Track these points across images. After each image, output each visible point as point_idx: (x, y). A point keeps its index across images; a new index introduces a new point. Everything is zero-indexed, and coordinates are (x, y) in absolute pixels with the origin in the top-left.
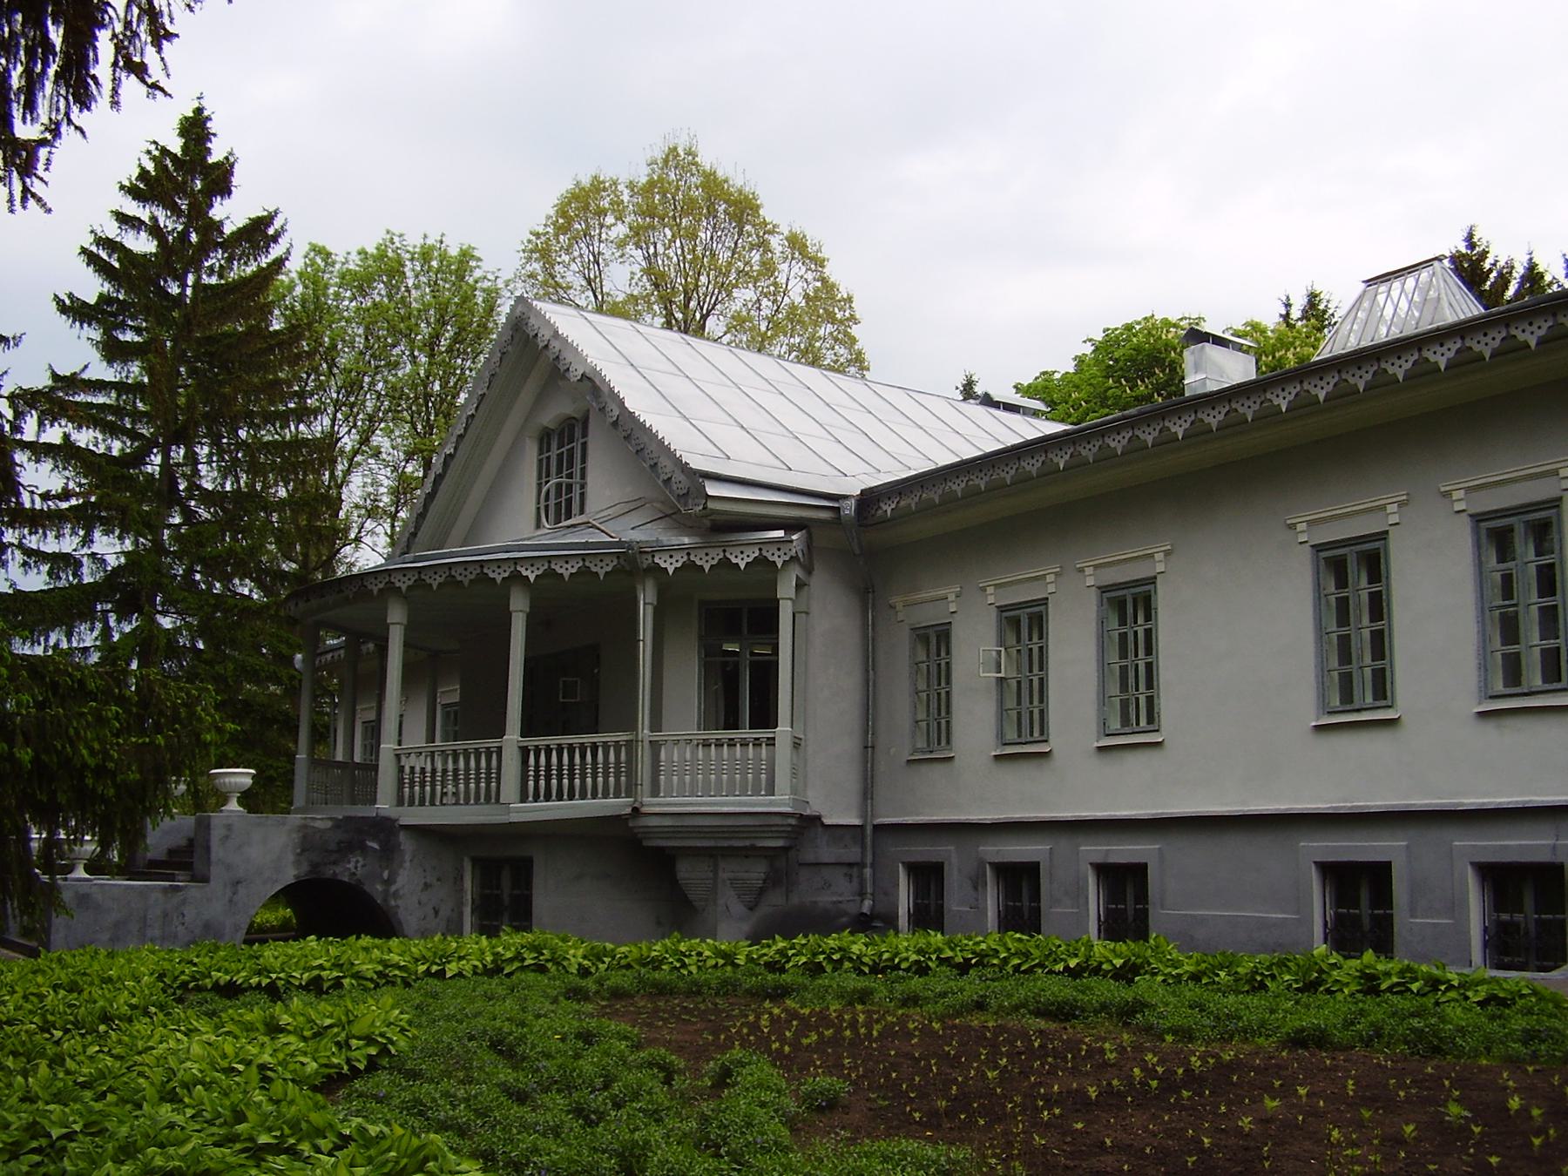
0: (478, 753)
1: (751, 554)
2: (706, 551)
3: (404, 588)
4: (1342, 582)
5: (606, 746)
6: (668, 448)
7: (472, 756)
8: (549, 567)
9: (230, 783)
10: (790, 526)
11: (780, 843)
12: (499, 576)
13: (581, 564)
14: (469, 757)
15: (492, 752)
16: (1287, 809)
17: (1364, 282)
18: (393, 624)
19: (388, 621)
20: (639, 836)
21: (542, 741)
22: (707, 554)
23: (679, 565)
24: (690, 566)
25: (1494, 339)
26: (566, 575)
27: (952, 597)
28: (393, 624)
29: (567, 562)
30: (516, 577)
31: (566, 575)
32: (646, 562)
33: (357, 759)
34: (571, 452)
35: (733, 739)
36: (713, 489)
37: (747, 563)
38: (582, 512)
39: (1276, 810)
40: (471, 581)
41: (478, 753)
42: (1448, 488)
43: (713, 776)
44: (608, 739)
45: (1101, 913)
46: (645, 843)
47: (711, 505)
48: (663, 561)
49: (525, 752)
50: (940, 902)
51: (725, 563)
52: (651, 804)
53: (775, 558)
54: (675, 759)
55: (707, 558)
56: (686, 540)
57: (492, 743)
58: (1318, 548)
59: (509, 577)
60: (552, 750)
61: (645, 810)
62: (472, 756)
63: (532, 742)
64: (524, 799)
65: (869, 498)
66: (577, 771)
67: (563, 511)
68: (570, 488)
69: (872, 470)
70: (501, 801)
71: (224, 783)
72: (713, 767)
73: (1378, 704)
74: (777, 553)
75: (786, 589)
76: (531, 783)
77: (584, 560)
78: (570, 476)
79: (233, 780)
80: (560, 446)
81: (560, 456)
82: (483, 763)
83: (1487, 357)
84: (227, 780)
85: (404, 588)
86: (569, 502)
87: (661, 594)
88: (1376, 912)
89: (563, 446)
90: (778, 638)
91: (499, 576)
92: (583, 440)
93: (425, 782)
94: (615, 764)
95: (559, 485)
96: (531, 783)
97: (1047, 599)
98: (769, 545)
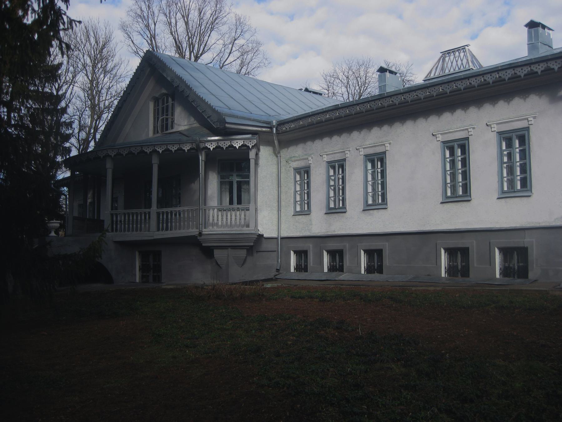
0: (133, 214)
1: (240, 143)
2: (224, 142)
3: (113, 156)
4: (452, 154)
5: (163, 213)
6: (210, 105)
7: (131, 215)
8: (167, 147)
9: (52, 226)
10: (254, 133)
11: (252, 244)
12: (148, 151)
13: (178, 146)
14: (130, 216)
15: (130, 214)
16: (293, 236)
17: (441, 53)
18: (154, 163)
19: (250, 158)
20: (201, 242)
21: (165, 210)
22: (224, 143)
23: (214, 147)
24: (218, 147)
25: (525, 71)
26: (173, 150)
27: (310, 158)
28: (154, 163)
29: (173, 146)
30: (155, 151)
31: (173, 150)
32: (202, 145)
33: (96, 218)
34: (167, 106)
35: (239, 208)
36: (228, 120)
37: (126, 154)
38: (172, 128)
39: (271, 236)
40: (175, 150)
41: (133, 214)
42: (490, 123)
43: (195, 222)
44: (146, 211)
45: (365, 266)
46: (203, 245)
47: (227, 125)
48: (208, 145)
49: (158, 214)
50: (306, 264)
51: (231, 146)
52: (205, 231)
53: (249, 145)
54: (190, 216)
55: (225, 144)
56: (216, 138)
57: (147, 210)
58: (444, 142)
59: (164, 150)
60: (138, 214)
61: (203, 233)
62: (131, 215)
63: (161, 210)
64: (158, 230)
65: (281, 123)
66: (135, 222)
67: (165, 127)
68: (167, 119)
69: (278, 114)
70: (151, 231)
71: (50, 226)
72: (191, 219)
73: (523, 189)
74: (250, 143)
75: (252, 154)
76: (161, 225)
77: (179, 145)
78: (167, 115)
79: (53, 225)
80: (163, 104)
81: (163, 108)
82: (131, 218)
83: (462, 90)
84: (51, 225)
85: (113, 156)
86: (167, 125)
87: (207, 155)
88: (155, 274)
89: (166, 106)
90: (250, 173)
91: (148, 151)
92: (167, 104)
93: (164, 222)
94: (166, 219)
95: (163, 119)
96: (161, 225)
97: (346, 159)
98: (247, 140)
